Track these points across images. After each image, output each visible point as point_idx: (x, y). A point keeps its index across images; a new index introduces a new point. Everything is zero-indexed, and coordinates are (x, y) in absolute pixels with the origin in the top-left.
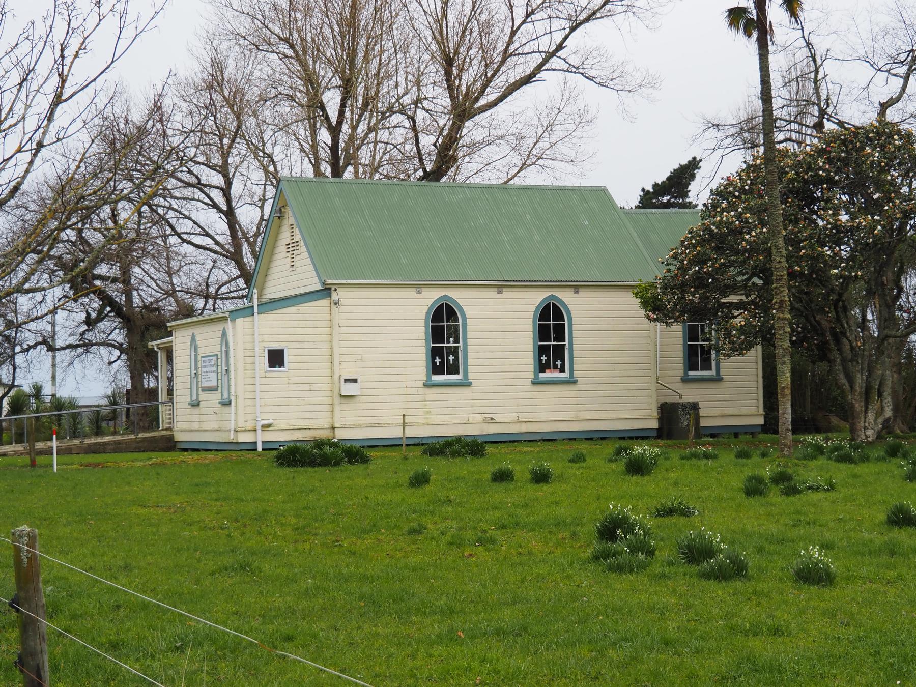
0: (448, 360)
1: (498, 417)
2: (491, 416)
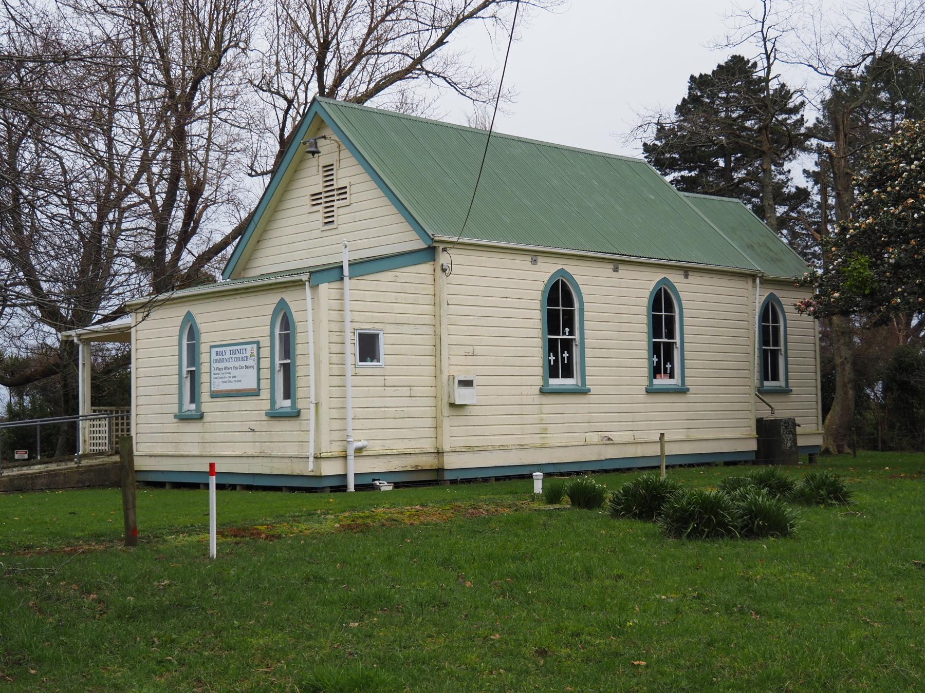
0: (563, 358)
1: (617, 437)
2: (608, 434)
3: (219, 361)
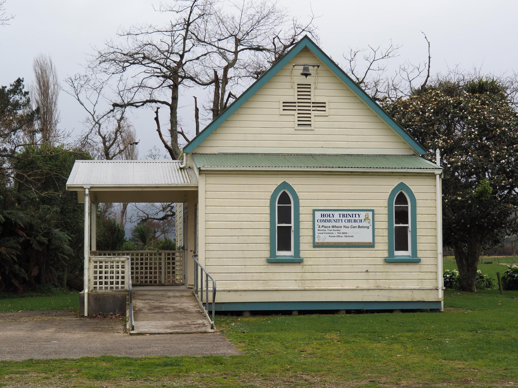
3: (321, 221)
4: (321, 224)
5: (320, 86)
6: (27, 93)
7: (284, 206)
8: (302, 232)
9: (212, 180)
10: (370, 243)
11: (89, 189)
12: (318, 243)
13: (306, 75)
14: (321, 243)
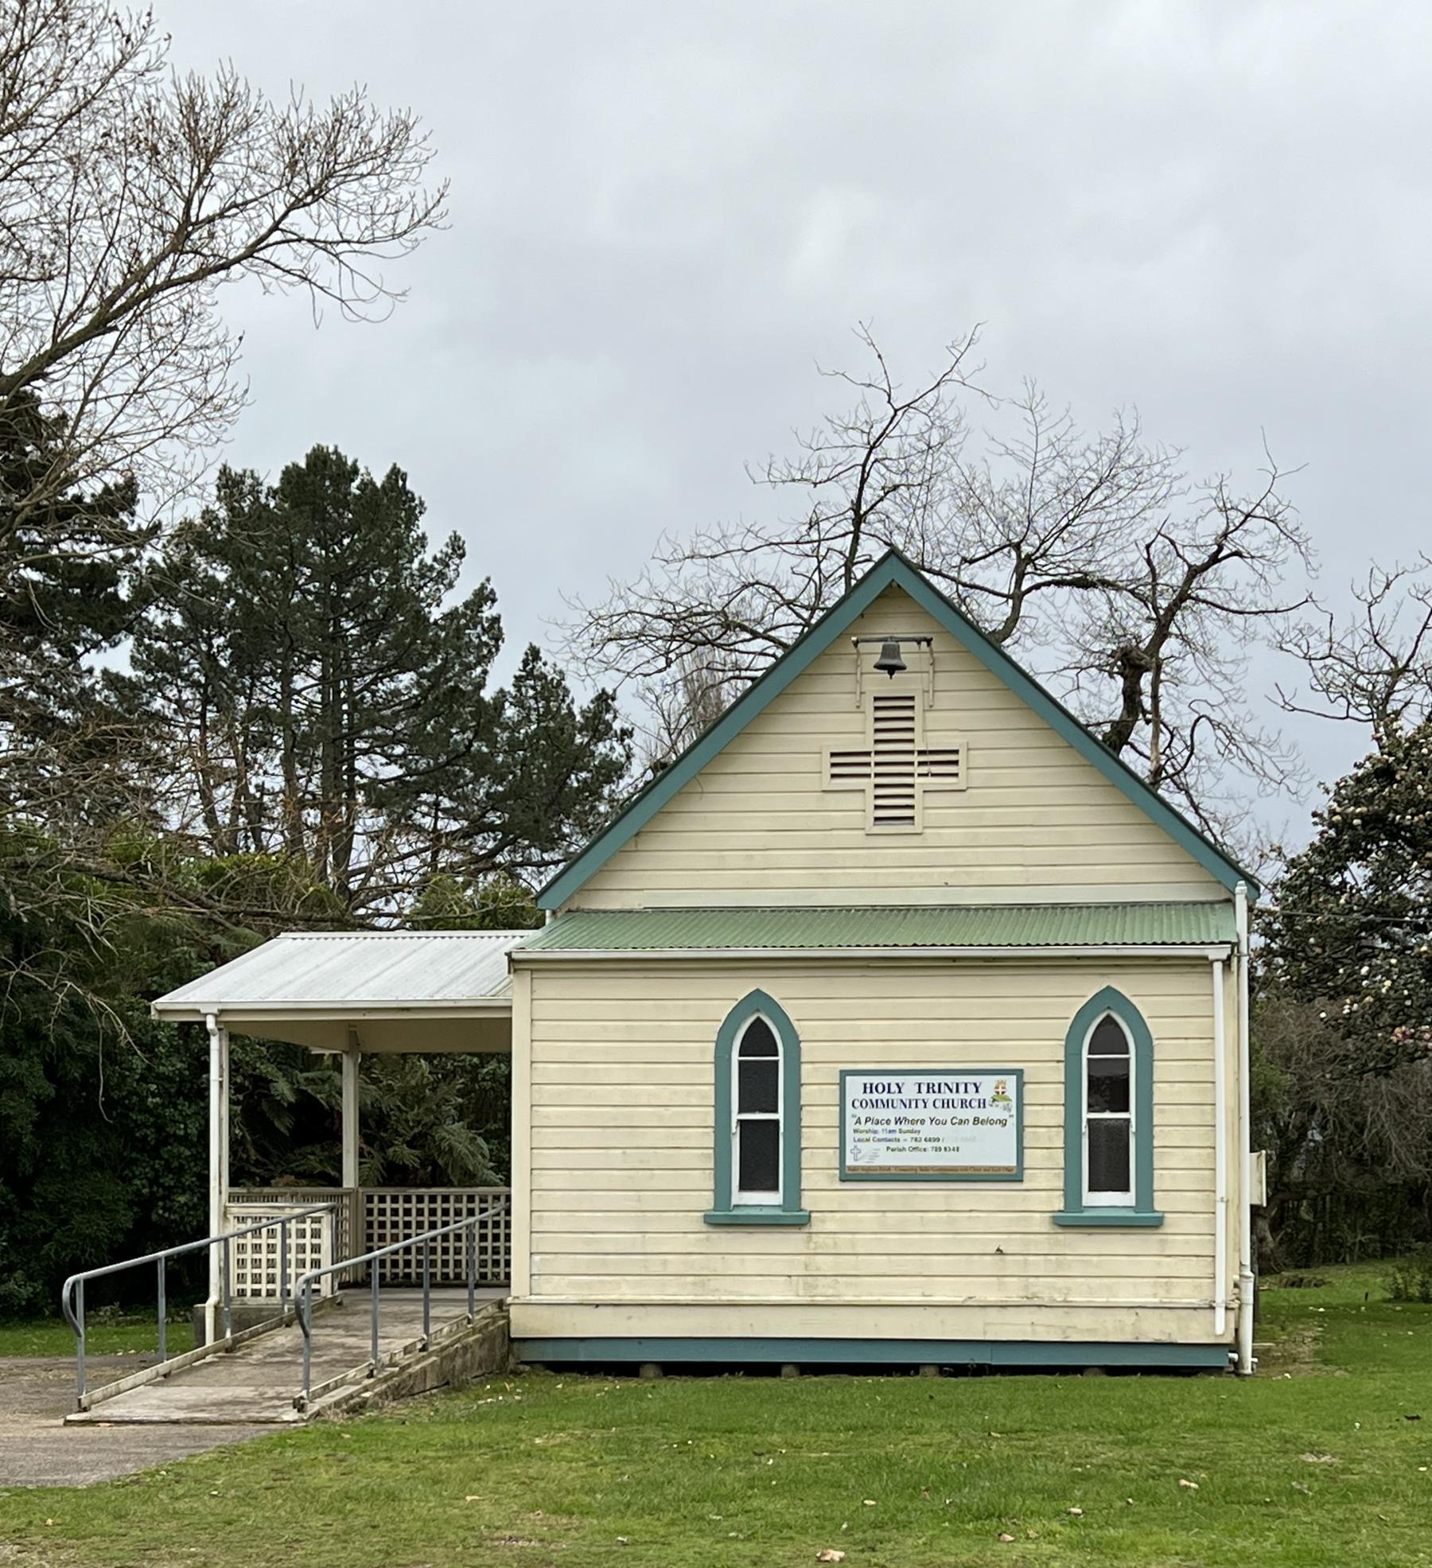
4: (863, 1113)
5: (943, 700)
6: (626, 733)
7: (759, 1062)
8: (808, 1138)
9: (549, 987)
10: (1008, 1169)
11: (216, 1016)
12: (854, 1168)
13: (892, 670)
14: (863, 1168)
